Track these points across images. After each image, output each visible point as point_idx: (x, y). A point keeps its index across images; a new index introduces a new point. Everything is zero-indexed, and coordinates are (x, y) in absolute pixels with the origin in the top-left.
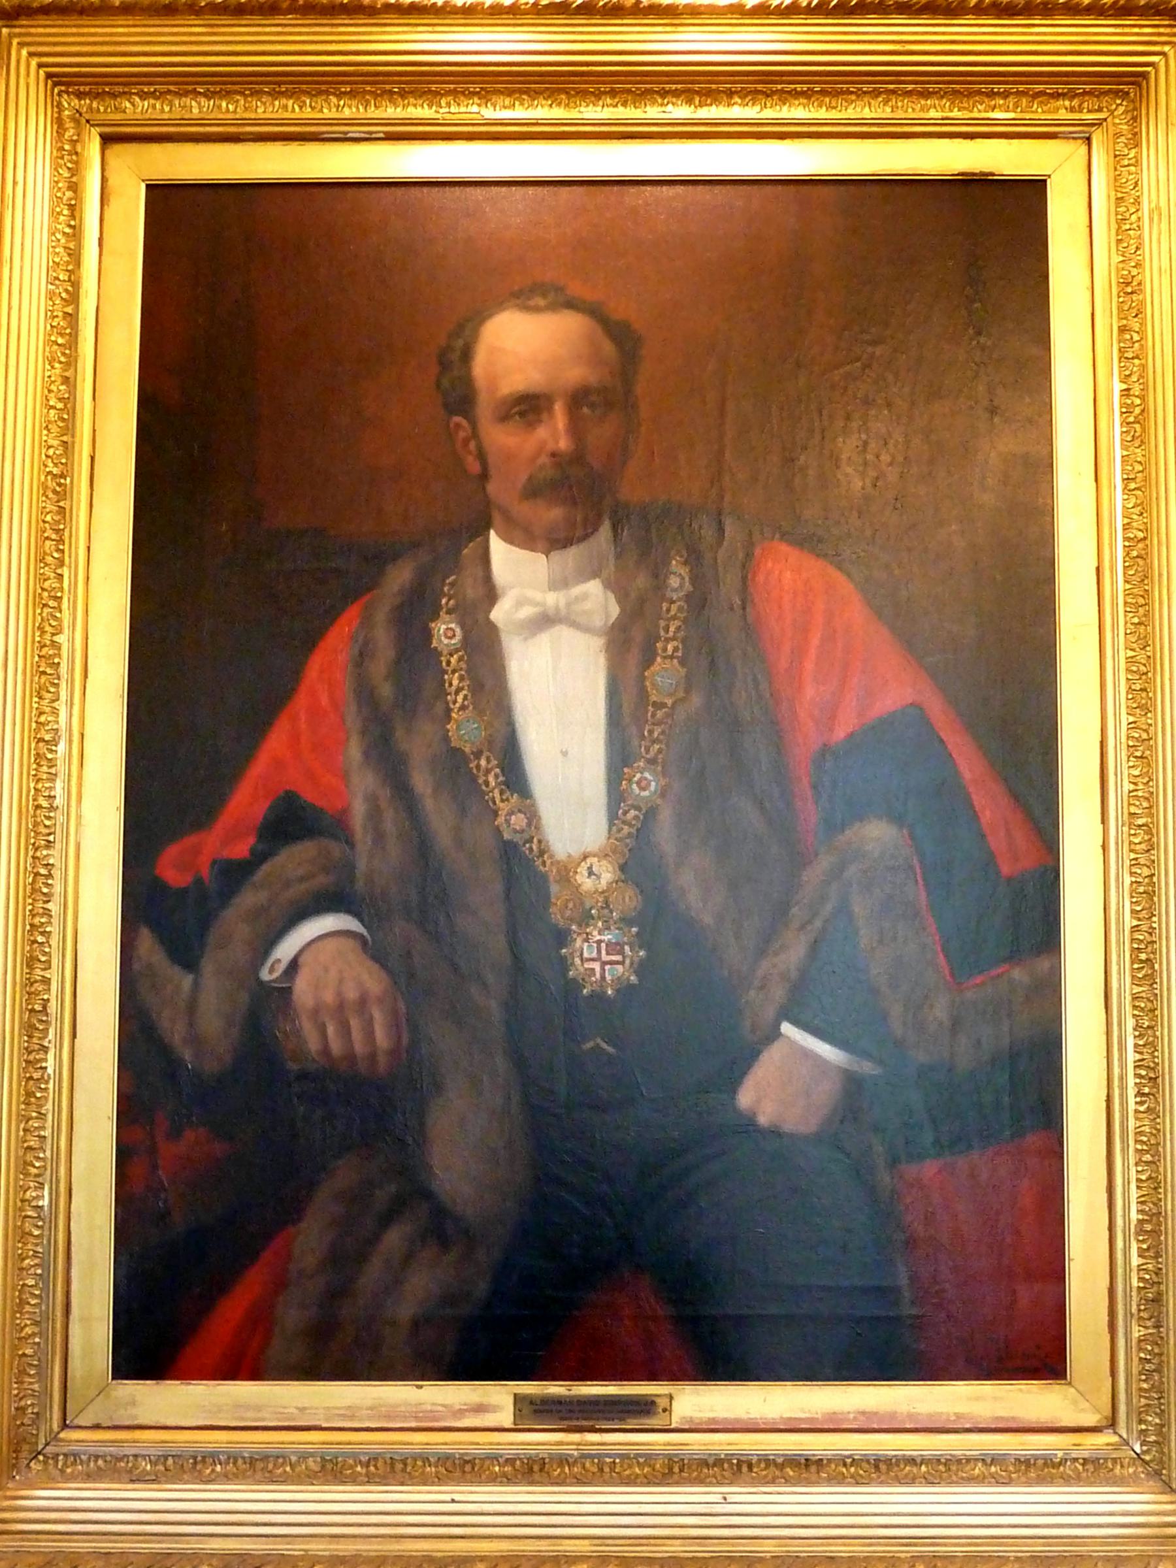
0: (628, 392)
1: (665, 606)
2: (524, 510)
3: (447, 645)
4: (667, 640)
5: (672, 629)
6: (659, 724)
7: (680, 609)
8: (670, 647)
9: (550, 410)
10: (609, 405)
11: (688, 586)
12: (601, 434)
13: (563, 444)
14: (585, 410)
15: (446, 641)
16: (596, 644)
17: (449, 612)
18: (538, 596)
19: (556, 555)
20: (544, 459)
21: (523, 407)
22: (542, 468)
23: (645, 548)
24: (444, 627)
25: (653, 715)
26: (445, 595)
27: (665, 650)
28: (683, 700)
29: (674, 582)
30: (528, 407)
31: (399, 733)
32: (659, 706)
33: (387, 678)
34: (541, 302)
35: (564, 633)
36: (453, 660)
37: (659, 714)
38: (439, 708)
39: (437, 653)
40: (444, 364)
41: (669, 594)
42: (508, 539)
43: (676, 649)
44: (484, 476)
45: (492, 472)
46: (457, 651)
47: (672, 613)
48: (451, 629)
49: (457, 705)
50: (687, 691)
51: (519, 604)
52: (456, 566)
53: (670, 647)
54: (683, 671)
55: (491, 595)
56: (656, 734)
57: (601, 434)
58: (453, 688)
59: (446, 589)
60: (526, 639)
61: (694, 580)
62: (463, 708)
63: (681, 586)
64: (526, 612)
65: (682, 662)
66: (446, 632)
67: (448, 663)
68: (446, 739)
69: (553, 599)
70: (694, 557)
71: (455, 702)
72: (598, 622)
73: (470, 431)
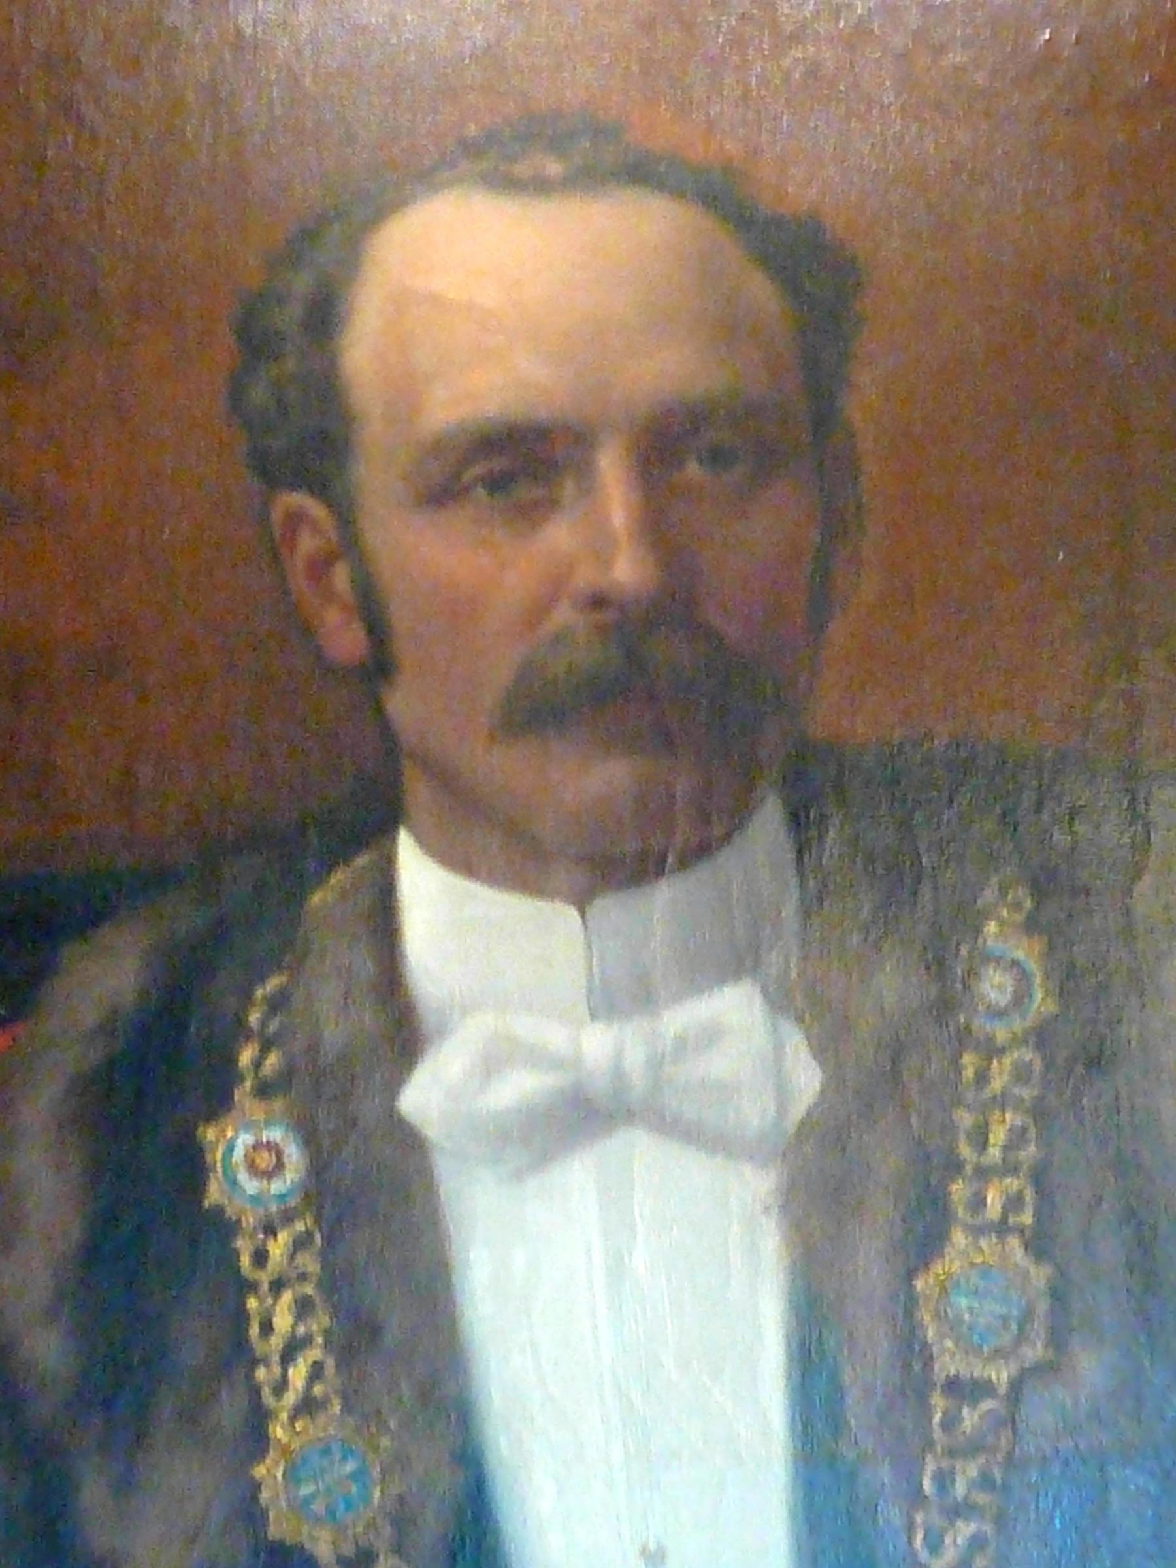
0: (824, 417)
1: (969, 1062)
2: (501, 767)
3: (256, 1199)
4: (983, 1174)
5: (998, 1136)
6: (974, 1448)
7: (1021, 1074)
8: (994, 1200)
9: (585, 470)
10: (768, 460)
11: (1041, 1003)
12: (755, 537)
13: (628, 570)
14: (693, 470)
15: (251, 1186)
16: (755, 1186)
17: (263, 1091)
18: (555, 1037)
19: (611, 908)
20: (564, 615)
21: (499, 464)
22: (557, 639)
23: (897, 877)
24: (244, 1140)
25: (950, 1423)
26: (248, 1035)
27: (978, 1203)
28: (1048, 1370)
29: (995, 986)
30: (516, 463)
31: (93, 1492)
32: (962, 1390)
33: (52, 1314)
34: (554, 168)
35: (639, 1151)
36: (278, 1248)
37: (970, 1418)
38: (229, 1411)
39: (223, 1228)
40: (256, 343)
41: (981, 1025)
42: (456, 858)
43: (1014, 1203)
44: (380, 666)
45: (404, 649)
46: (288, 1217)
47: (997, 1084)
48: (270, 1146)
49: (290, 1398)
50: (1057, 1339)
51: (492, 1064)
52: (285, 944)
53: (994, 1200)
54: (1040, 1275)
55: (401, 1033)
56: (960, 1489)
57: (755, 537)
58: (276, 1342)
59: (254, 1018)
60: (518, 1176)
61: (1067, 981)
62: (308, 1406)
63: (1020, 999)
64: (518, 1088)
65: (1039, 1244)
66: (252, 1158)
67: (260, 1258)
68: (250, 1512)
69: (598, 1045)
70: (1056, 895)
71: (281, 1386)
72: (754, 1113)
73: (333, 536)
